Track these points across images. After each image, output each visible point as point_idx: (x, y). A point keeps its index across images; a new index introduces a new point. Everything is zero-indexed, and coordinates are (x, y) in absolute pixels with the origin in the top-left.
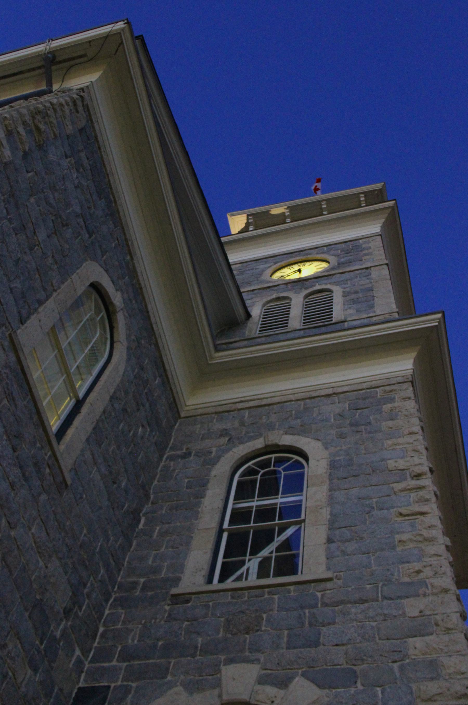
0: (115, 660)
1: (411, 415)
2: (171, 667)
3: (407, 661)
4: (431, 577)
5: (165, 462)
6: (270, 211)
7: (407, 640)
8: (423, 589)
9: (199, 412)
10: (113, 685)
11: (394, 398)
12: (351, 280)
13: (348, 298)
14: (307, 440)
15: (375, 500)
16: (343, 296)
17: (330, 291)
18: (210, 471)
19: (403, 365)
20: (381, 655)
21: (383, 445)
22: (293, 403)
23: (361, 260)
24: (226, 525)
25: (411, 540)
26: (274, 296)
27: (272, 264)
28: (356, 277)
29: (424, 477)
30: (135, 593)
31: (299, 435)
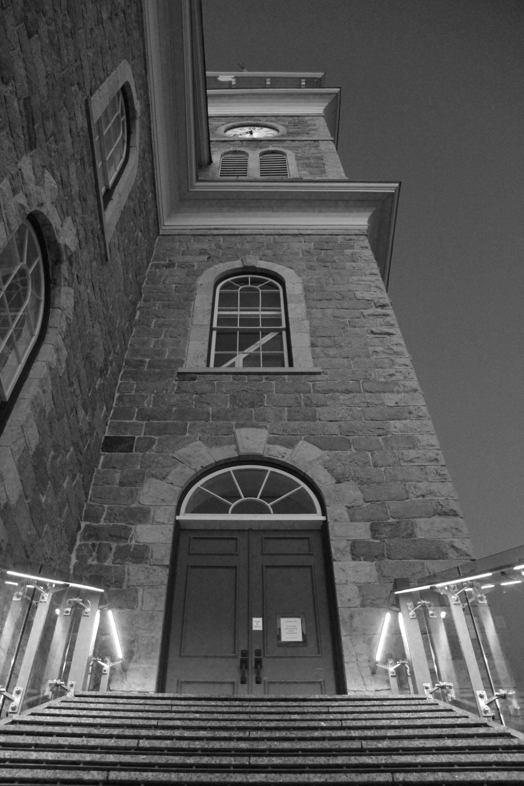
0: (134, 418)
1: (369, 260)
2: (188, 427)
3: (389, 435)
4: (402, 380)
5: (151, 269)
7: (387, 421)
8: (397, 387)
9: (176, 232)
10: (137, 437)
11: (354, 245)
12: (302, 148)
13: (301, 162)
14: (281, 267)
15: (348, 320)
17: (284, 154)
18: (195, 280)
19: (359, 221)
20: (368, 430)
21: (349, 280)
22: (263, 236)
23: (309, 134)
24: (215, 325)
26: (232, 149)
27: (224, 123)
29: (387, 308)
30: (144, 369)
31: (272, 262)
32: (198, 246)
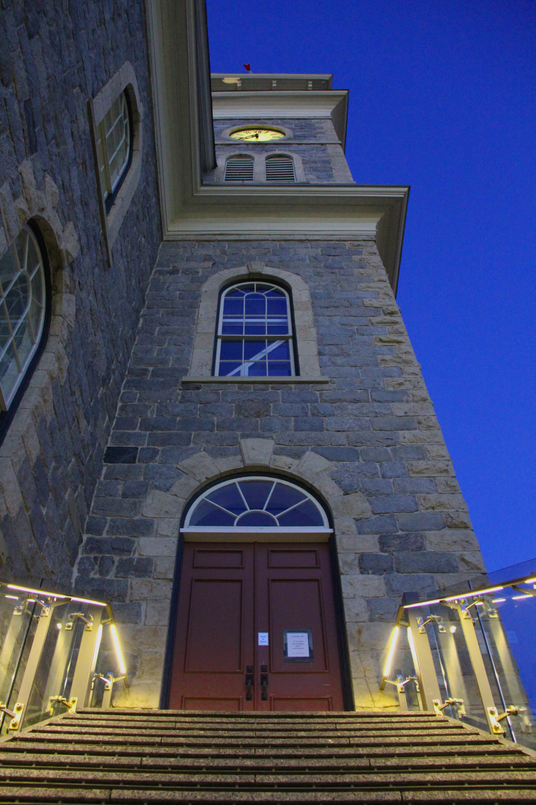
0: (137, 428)
1: (378, 266)
2: (192, 437)
3: (398, 446)
4: (411, 389)
5: (154, 275)
6: (223, 79)
8: (406, 397)
9: (180, 238)
10: (140, 447)
11: (362, 251)
13: (307, 166)
14: (288, 273)
16: (303, 164)
17: (290, 157)
19: (367, 226)
20: (377, 441)
23: (316, 137)
24: (220, 333)
25: (391, 360)
26: (237, 153)
28: (313, 150)
29: (396, 315)
30: (147, 378)
31: (279, 268)
32: (203, 252)
